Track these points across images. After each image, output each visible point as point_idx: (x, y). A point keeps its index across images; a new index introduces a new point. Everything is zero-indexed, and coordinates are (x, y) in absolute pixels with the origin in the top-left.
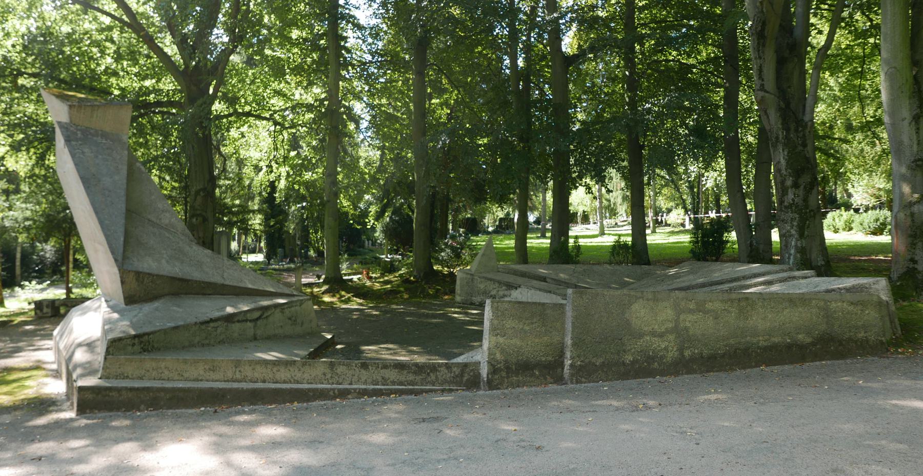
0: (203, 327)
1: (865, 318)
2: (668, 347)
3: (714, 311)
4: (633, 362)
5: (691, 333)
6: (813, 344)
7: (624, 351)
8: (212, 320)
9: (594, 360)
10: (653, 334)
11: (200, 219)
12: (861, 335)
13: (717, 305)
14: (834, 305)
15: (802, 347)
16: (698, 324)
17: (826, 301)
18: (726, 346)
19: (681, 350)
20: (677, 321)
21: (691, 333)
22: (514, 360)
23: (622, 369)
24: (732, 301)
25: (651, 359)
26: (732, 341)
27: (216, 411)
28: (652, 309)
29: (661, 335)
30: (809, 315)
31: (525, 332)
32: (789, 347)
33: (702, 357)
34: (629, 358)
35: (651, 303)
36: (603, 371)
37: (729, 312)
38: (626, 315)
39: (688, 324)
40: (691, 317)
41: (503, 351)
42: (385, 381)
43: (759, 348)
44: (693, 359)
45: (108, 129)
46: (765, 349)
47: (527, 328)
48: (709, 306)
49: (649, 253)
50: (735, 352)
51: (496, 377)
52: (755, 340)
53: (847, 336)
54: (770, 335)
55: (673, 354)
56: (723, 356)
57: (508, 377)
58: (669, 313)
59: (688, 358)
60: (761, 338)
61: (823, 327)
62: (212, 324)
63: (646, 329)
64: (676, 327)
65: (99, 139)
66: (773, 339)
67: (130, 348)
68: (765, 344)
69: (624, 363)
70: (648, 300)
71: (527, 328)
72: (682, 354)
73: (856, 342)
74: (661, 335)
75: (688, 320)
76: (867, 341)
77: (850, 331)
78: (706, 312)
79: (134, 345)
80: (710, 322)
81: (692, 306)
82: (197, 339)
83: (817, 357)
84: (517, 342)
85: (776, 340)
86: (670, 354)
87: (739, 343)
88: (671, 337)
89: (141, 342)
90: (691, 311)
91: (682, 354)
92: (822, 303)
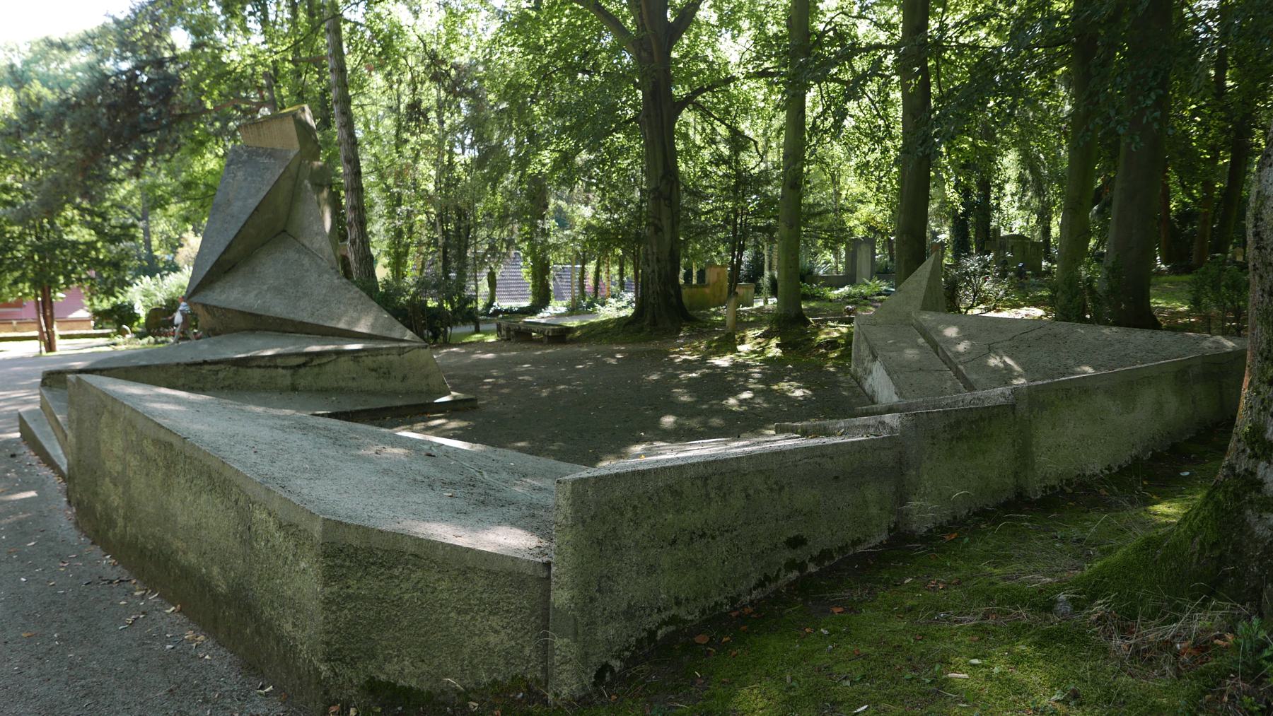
0: (193, 369)
8: (205, 362)
11: (652, 229)
45: (279, 147)
62: (207, 367)
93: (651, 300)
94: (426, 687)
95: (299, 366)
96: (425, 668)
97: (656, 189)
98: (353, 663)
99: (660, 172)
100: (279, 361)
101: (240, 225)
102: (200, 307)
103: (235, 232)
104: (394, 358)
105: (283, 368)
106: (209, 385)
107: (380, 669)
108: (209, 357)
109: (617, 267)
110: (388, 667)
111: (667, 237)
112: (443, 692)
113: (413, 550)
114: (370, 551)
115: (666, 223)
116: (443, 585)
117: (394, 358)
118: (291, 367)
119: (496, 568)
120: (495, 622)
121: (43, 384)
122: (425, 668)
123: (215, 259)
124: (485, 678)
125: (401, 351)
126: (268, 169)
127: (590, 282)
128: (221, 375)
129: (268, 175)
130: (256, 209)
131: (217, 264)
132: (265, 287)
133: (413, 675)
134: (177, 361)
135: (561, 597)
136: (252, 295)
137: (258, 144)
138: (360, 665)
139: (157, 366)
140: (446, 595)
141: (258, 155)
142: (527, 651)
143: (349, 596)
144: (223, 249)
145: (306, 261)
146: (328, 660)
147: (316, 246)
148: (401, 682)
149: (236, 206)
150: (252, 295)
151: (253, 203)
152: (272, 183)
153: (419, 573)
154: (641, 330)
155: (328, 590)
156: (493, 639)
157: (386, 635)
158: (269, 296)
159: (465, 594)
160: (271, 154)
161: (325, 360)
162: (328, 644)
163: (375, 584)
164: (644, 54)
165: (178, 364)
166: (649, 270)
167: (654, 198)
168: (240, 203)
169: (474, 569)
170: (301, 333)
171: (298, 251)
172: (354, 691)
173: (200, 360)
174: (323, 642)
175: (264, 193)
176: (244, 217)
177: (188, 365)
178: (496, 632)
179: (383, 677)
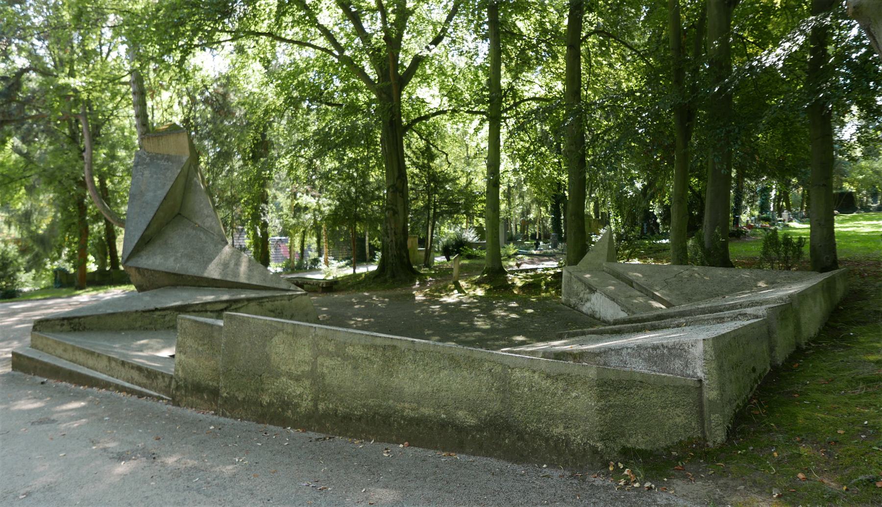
0: (147, 314)
1: (570, 403)
2: (301, 393)
3: (354, 358)
4: (271, 404)
5: (327, 382)
6: (478, 428)
7: (262, 390)
8: (156, 309)
9: (237, 394)
10: (290, 375)
11: (391, 212)
12: (558, 430)
13: (359, 351)
14: (518, 374)
15: (461, 429)
16: (337, 374)
17: (505, 367)
18: (364, 406)
19: (315, 401)
20: (314, 364)
21: (327, 382)
22: (190, 380)
23: (260, 409)
24: (375, 347)
25: (286, 405)
26: (371, 402)
27: (754, 370)
28: (291, 345)
29: (298, 379)
30: (476, 383)
31: (199, 352)
32: (443, 425)
33: (336, 416)
34: (266, 399)
35: (290, 337)
36: (243, 408)
37: (371, 362)
38: (267, 349)
39: (325, 371)
40: (329, 362)
41: (183, 369)
42: (131, 380)
43: (403, 417)
44: (326, 415)
45: (173, 154)
46: (411, 421)
47: (200, 349)
48: (349, 350)
49: (838, 251)
50: (374, 417)
51: (178, 393)
52: (399, 406)
53: (533, 426)
54: (418, 403)
55: (306, 405)
56: (360, 419)
57: (186, 396)
58: (305, 353)
59: (321, 412)
60: (406, 405)
61: (496, 406)
62: (158, 313)
63: (283, 368)
64: (313, 371)
65: (162, 162)
66: (422, 410)
67: (59, 327)
68: (412, 414)
69: (261, 405)
70: (287, 334)
71: (200, 349)
72: (316, 405)
73: (547, 440)
74: (298, 379)
75: (327, 364)
76: (568, 442)
77: (539, 421)
78: (346, 357)
79: (62, 325)
80: (348, 372)
81: (331, 348)
82: (139, 324)
83: (481, 449)
84: (192, 361)
85: (427, 411)
86: (304, 404)
87: (380, 406)
88: (307, 383)
89: (70, 324)
90: (330, 355)
91: (316, 405)
92: (499, 369)
93: (390, 260)
94: (649, 448)
95: (222, 310)
96: (648, 438)
97: (393, 186)
98: (614, 441)
99: (396, 174)
100: (208, 307)
101: (155, 209)
102: (133, 270)
103: (152, 215)
104: (285, 302)
105: (211, 312)
106: (158, 326)
107: (627, 441)
108: (159, 306)
109: (315, 239)
110: (632, 440)
111: (401, 218)
112: (658, 450)
113: (640, 379)
114: (620, 382)
115: (400, 208)
116: (654, 395)
117: (285, 302)
118: (217, 311)
119: (678, 384)
120: (678, 411)
121: (35, 328)
122: (648, 438)
123: (140, 234)
124: (676, 440)
125: (290, 298)
126: (168, 169)
127: (297, 249)
128: (167, 318)
129: (169, 174)
130: (165, 198)
131: (142, 238)
132: (179, 255)
133: (643, 443)
134: (134, 309)
135: (711, 394)
136: (172, 259)
137: (157, 151)
138: (618, 441)
139: (121, 313)
140: (655, 400)
141: (158, 159)
142: (693, 424)
143: (611, 406)
144: (145, 227)
145: (202, 235)
146: (603, 440)
147: (208, 224)
148: (638, 447)
149: (149, 195)
150: (172, 259)
151: (161, 194)
152: (174, 179)
153: (643, 391)
154: (385, 281)
155: (600, 404)
156: (678, 420)
157: (630, 423)
158: (184, 261)
159: (663, 399)
160: (169, 158)
161: (239, 305)
162: (601, 431)
163: (623, 398)
164: (384, 96)
165: (137, 311)
166: (389, 240)
167: (394, 192)
168: (151, 194)
169: (667, 386)
170: (212, 286)
171: (194, 228)
172: (615, 454)
173: (152, 307)
174: (598, 431)
175: (169, 187)
176: (157, 204)
177: (144, 312)
178: (679, 416)
179: (629, 446)
